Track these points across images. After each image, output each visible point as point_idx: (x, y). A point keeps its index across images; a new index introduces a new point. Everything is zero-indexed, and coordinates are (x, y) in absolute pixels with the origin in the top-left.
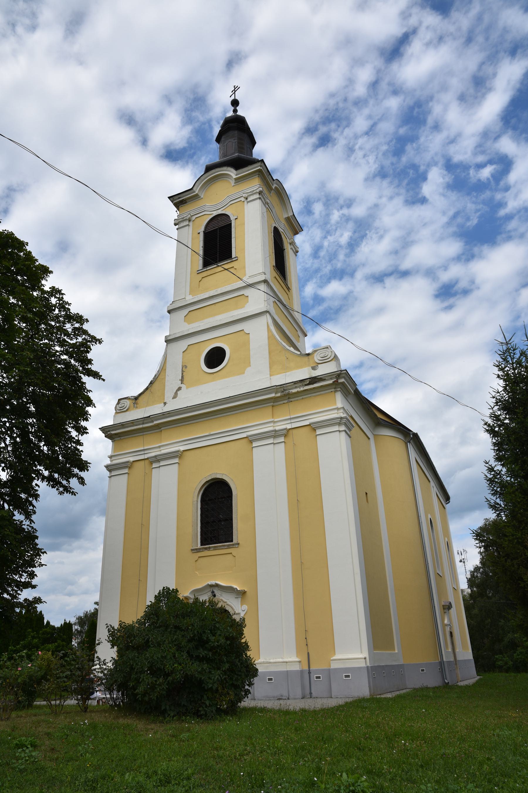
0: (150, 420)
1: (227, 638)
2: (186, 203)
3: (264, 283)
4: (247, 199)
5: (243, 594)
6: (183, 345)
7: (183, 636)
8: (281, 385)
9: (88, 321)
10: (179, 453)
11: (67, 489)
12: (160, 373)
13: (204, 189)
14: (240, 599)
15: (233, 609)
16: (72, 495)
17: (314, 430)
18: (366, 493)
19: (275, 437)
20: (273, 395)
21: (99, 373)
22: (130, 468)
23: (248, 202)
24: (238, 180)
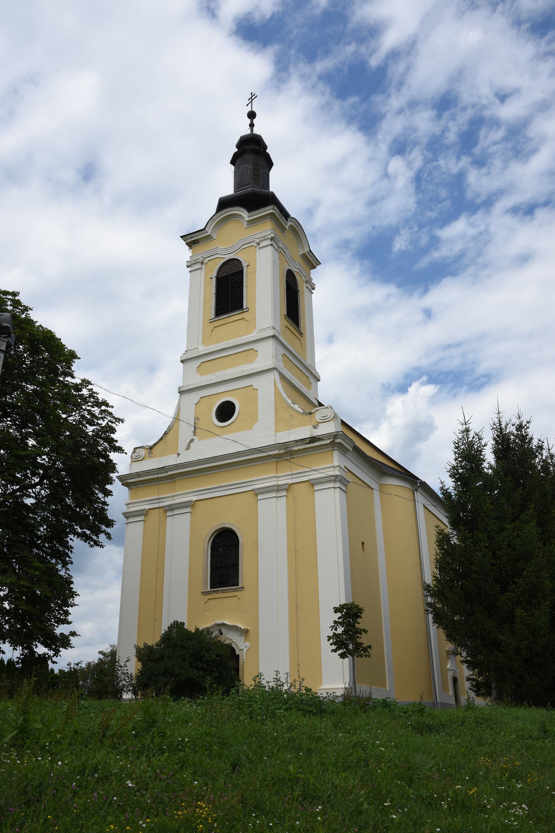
0: (164, 471)
1: (217, 656)
2: (198, 243)
3: (273, 338)
4: (259, 244)
5: (245, 632)
6: (196, 396)
7: (187, 652)
8: (284, 443)
9: (113, 407)
10: (192, 503)
11: (97, 543)
12: (173, 424)
14: (243, 637)
15: (237, 645)
16: (101, 547)
17: (313, 485)
18: (363, 543)
19: (278, 491)
20: (277, 452)
22: (146, 515)
23: (260, 248)
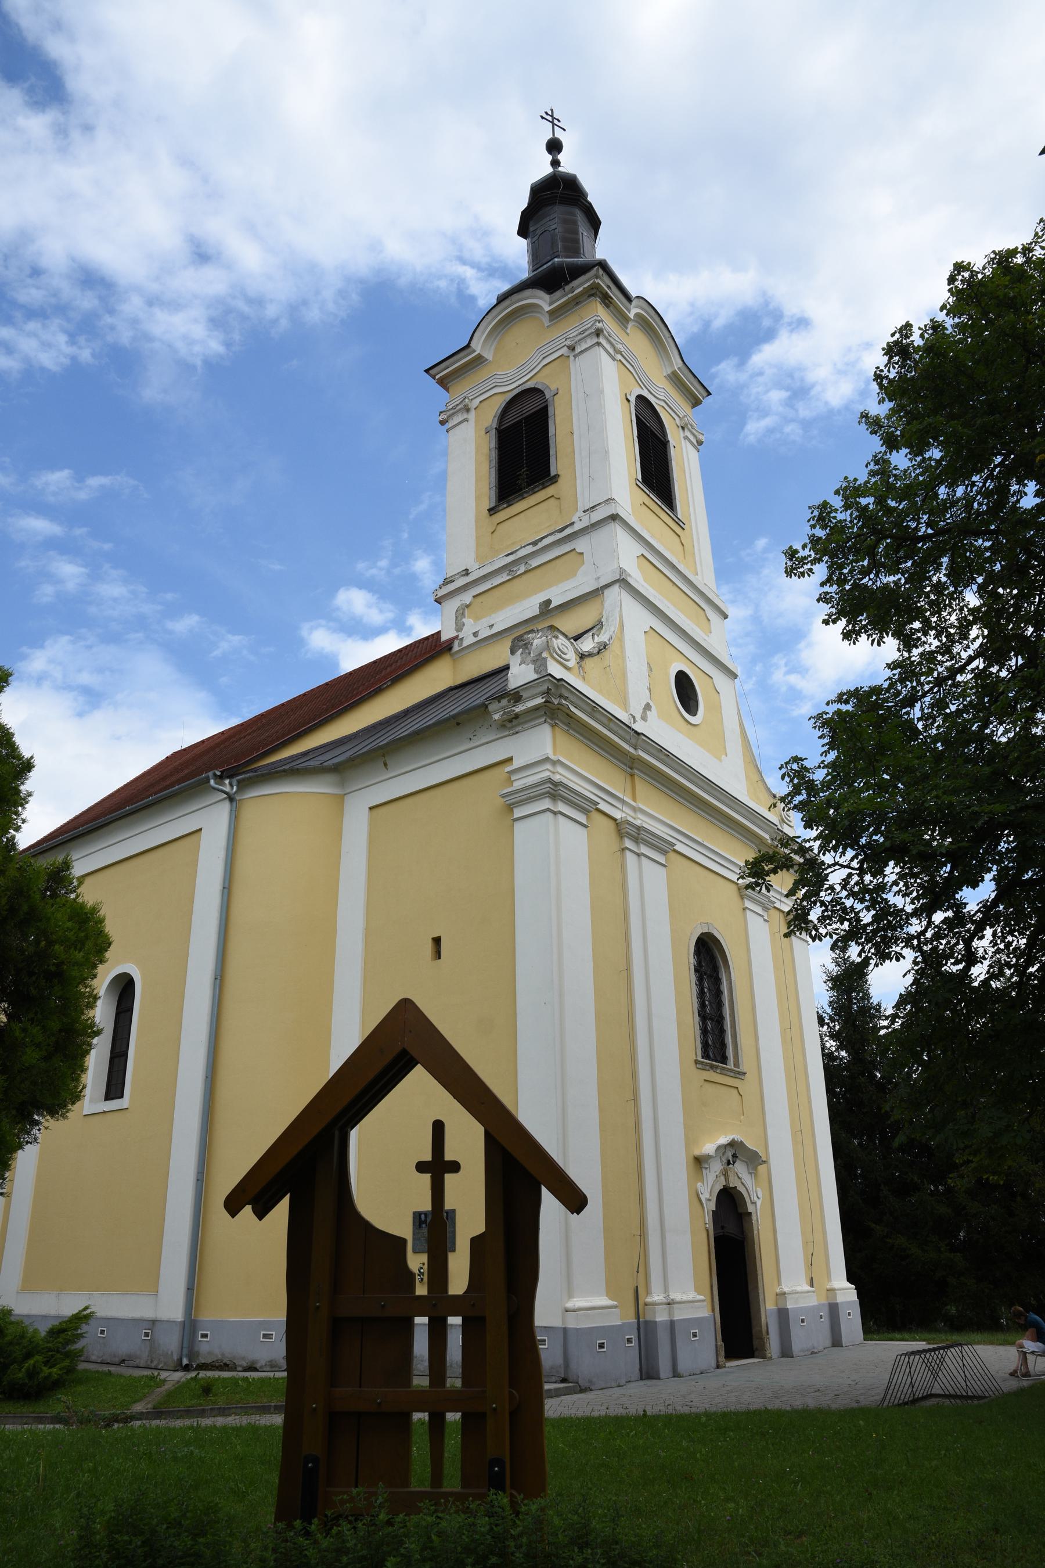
2: (608, 306)
4: (573, 349)
13: (495, 339)
21: (898, 452)
23: (575, 356)
24: (555, 314)
